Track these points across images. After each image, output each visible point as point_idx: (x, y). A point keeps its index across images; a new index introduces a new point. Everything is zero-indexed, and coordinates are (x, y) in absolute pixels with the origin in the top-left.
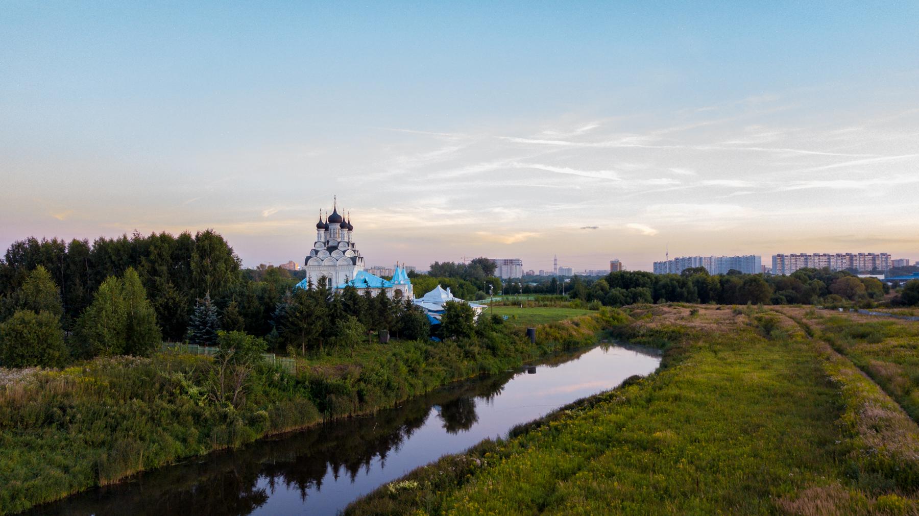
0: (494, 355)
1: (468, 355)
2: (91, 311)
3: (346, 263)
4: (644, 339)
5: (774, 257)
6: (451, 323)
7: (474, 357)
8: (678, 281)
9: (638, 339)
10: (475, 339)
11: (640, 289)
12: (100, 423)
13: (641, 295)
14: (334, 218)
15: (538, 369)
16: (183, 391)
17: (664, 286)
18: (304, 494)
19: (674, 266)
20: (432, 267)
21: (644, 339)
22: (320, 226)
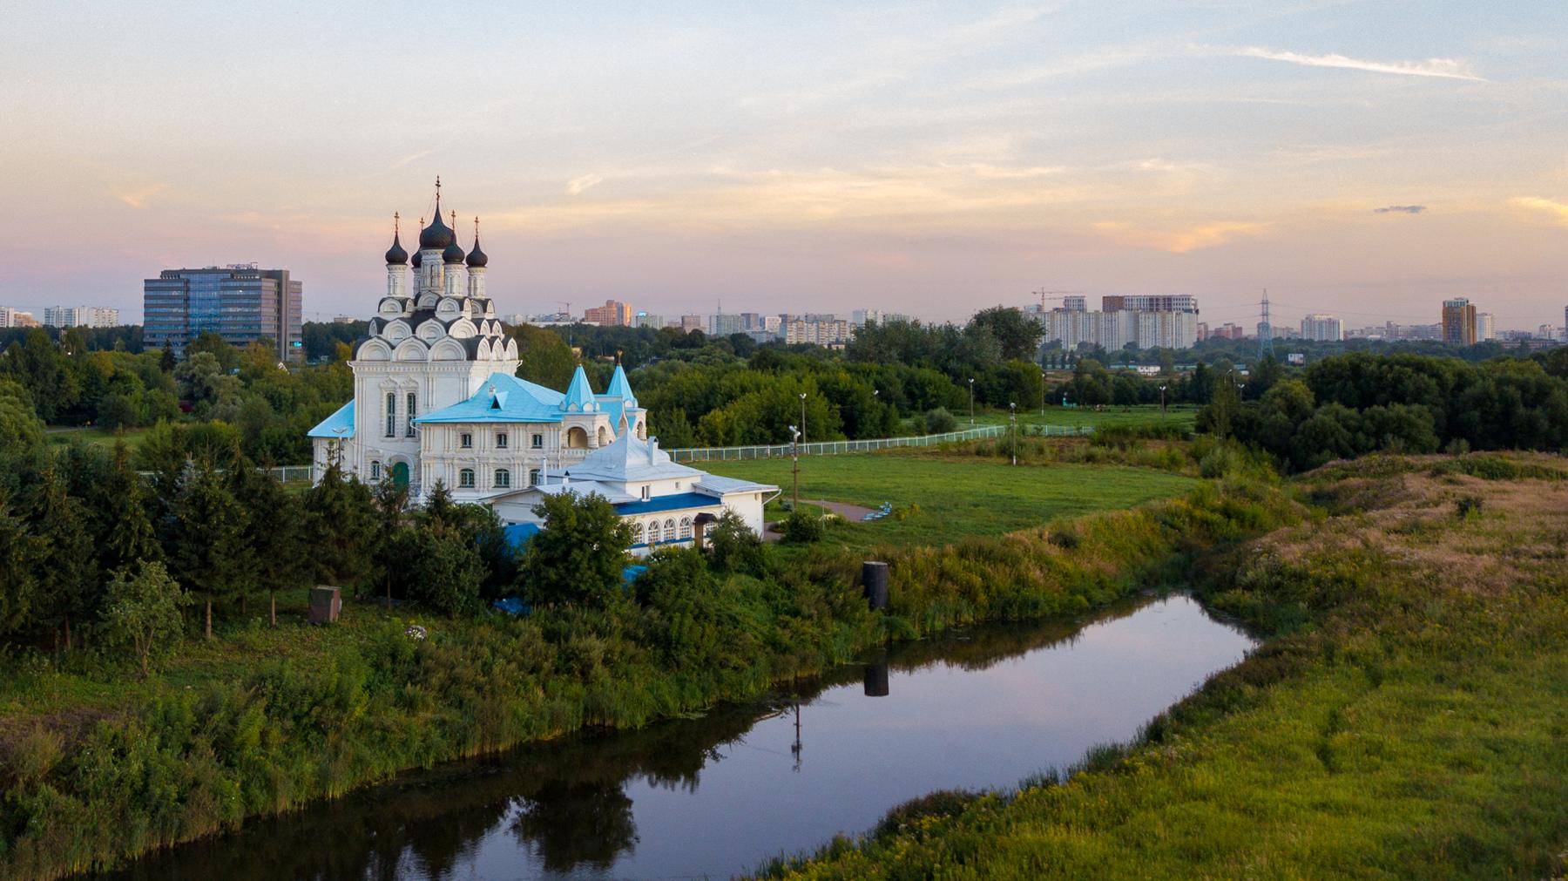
0: (667, 661)
3: (449, 355)
4: (1248, 598)
6: (550, 562)
8: (1523, 387)
9: (1233, 595)
10: (621, 609)
11: (1400, 409)
14: (437, 237)
15: (897, 679)
17: (1481, 401)
20: (858, 332)
21: (1248, 598)
22: (395, 257)
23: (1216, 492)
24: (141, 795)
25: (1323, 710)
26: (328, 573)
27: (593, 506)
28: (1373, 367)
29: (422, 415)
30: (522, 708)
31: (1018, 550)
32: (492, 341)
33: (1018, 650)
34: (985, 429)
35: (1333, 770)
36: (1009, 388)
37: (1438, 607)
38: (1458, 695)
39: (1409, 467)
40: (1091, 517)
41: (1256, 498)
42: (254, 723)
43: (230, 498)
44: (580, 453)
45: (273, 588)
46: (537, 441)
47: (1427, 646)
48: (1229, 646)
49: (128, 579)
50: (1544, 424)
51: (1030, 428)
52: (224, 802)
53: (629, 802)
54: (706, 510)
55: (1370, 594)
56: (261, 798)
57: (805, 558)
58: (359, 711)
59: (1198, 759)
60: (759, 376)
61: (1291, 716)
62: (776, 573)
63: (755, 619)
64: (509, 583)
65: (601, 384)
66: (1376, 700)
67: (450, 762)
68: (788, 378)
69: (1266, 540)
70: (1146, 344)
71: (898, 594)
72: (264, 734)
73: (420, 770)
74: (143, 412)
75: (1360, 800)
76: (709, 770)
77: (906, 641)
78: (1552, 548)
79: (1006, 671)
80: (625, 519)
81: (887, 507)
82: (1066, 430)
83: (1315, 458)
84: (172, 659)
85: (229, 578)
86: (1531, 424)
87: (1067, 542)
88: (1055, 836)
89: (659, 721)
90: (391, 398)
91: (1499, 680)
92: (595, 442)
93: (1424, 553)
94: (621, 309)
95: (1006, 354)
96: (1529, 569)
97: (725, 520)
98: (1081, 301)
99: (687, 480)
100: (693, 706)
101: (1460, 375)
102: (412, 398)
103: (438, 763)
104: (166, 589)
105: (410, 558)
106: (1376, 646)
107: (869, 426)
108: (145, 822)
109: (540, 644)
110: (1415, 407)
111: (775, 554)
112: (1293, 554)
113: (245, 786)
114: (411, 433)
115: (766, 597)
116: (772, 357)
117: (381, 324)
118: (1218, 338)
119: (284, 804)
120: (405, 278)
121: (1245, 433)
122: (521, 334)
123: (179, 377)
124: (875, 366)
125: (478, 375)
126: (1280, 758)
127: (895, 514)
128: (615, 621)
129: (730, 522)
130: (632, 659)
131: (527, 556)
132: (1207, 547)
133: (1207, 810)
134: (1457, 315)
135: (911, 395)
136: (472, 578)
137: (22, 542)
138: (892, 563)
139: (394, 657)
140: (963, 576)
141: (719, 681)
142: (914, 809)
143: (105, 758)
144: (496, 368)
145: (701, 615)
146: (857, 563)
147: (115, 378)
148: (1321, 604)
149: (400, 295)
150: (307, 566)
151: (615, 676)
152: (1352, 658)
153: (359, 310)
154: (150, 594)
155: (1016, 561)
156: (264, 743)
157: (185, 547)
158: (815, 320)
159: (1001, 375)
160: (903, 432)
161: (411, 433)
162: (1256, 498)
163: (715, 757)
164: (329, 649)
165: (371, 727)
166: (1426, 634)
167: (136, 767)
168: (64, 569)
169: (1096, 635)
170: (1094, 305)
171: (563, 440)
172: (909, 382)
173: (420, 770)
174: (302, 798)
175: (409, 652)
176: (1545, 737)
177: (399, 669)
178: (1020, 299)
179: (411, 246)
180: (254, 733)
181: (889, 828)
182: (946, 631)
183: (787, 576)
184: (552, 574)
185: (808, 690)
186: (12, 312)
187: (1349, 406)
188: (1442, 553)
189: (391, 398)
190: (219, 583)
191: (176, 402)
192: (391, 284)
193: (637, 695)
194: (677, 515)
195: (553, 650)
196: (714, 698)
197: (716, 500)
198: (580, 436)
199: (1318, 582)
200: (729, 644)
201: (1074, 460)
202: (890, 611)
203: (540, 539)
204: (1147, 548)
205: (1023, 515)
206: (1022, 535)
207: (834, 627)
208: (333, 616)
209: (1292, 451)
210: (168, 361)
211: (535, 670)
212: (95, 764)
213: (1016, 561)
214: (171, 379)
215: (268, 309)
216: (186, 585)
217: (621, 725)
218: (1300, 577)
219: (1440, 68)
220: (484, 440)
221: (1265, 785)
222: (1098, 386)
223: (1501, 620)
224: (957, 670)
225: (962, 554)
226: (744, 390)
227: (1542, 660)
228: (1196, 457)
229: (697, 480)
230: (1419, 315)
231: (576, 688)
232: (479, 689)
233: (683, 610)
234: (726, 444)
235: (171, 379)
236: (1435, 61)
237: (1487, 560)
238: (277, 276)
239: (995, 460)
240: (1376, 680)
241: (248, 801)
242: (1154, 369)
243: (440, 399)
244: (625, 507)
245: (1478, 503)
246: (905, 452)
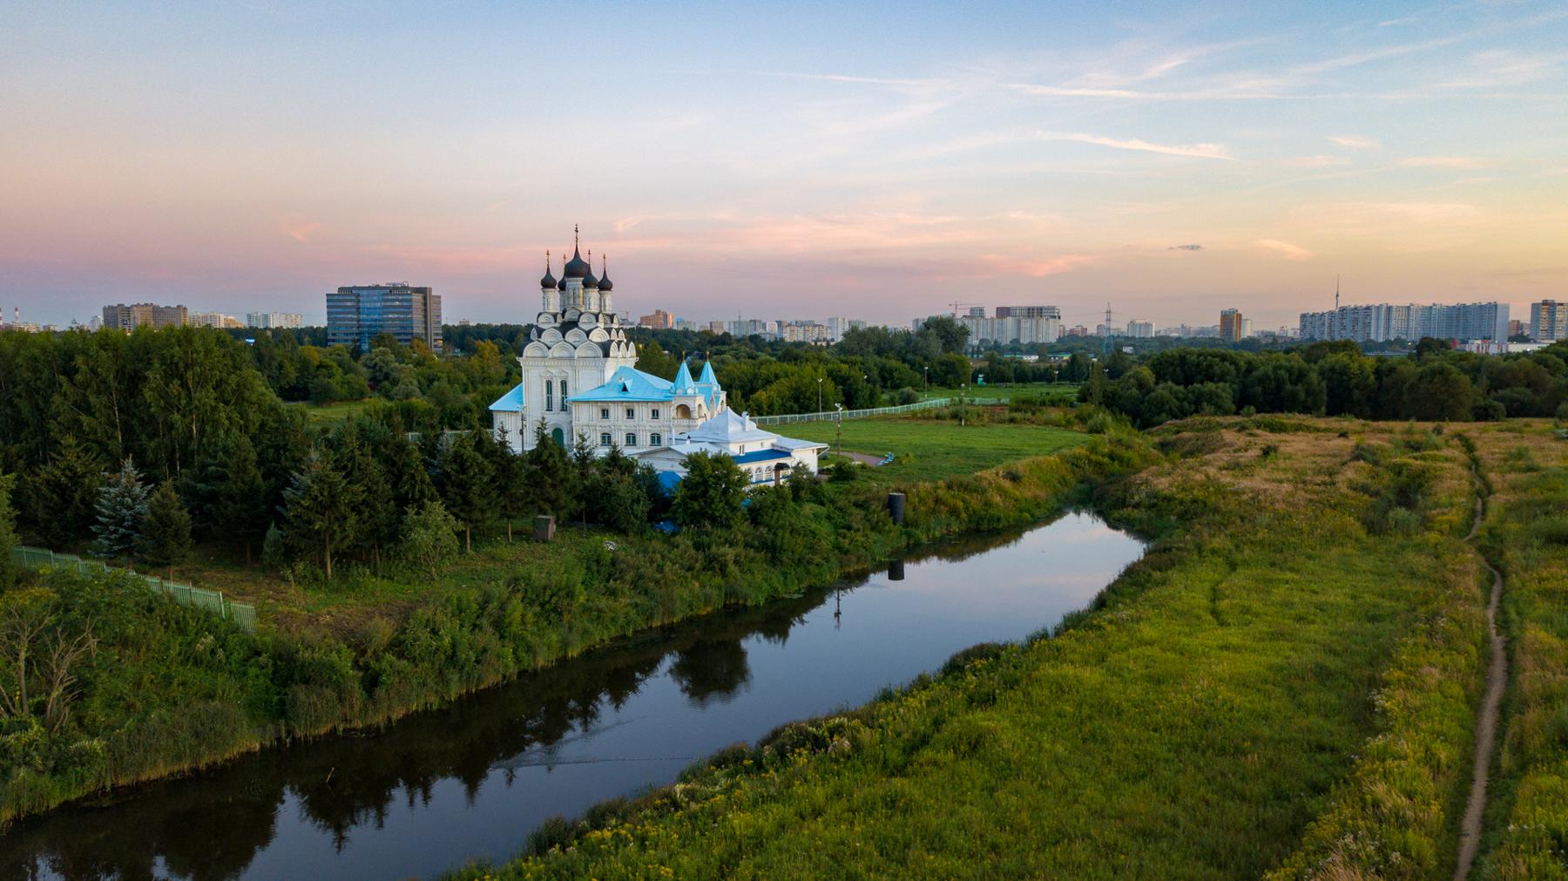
0: (774, 561)
1: (715, 565)
3: (590, 353)
4: (1135, 513)
5: (1535, 307)
6: (694, 498)
8: (1290, 371)
9: (1125, 512)
10: (741, 529)
11: (1210, 386)
13: (1211, 398)
14: (576, 268)
15: (909, 568)
17: (1261, 380)
18: (340, 839)
19: (1337, 323)
21: (1135, 513)
22: (547, 283)
23: (1104, 442)
24: (452, 658)
25: (1207, 585)
26: (547, 507)
27: (719, 460)
28: (1194, 358)
29: (571, 396)
30: (686, 594)
31: (985, 483)
32: (619, 343)
34: (937, 401)
35: (1222, 624)
36: (947, 373)
37: (1265, 518)
38: (1289, 575)
39: (1220, 425)
40: (1027, 460)
41: (1128, 447)
42: (516, 608)
43: (480, 458)
44: (685, 422)
45: (509, 517)
46: (655, 414)
47: (1261, 543)
49: (418, 513)
50: (1302, 395)
51: (966, 400)
52: (503, 664)
54: (782, 461)
55: (1216, 510)
56: (526, 659)
57: (849, 492)
58: (582, 599)
59: (1139, 620)
60: (786, 366)
61: (1189, 588)
62: (832, 502)
64: (666, 511)
65: (696, 373)
66: (1240, 578)
67: (643, 631)
68: (808, 368)
69: (1144, 475)
70: (1025, 340)
71: (911, 514)
72: (523, 616)
73: (624, 637)
74: (343, 391)
75: (1249, 643)
76: (796, 630)
77: (918, 544)
78: (1327, 479)
79: (975, 562)
80: (743, 467)
81: (890, 456)
82: (992, 400)
83: (1156, 419)
84: (447, 566)
85: (483, 511)
86: (1294, 395)
87: (1014, 478)
88: (1068, 670)
89: (773, 600)
90: (549, 384)
91: (1310, 564)
92: (695, 415)
93: (1245, 483)
94: (666, 316)
95: (946, 351)
96: (1314, 492)
97: (796, 468)
98: (981, 310)
99: (768, 440)
100: (792, 591)
101: (1249, 363)
102: (564, 384)
103: (636, 632)
104: (446, 520)
105: (587, 493)
106: (1229, 544)
107: (861, 400)
108: (456, 677)
109: (693, 552)
110: (1221, 384)
111: (828, 489)
112: (1163, 484)
113: (515, 652)
114: (564, 408)
115: (828, 517)
116: (791, 353)
117: (540, 332)
118: (1072, 336)
119: (541, 662)
120: (554, 296)
121: (1111, 402)
122: (634, 335)
123: (365, 365)
124: (859, 358)
125: (611, 368)
126: (1188, 616)
127: (898, 461)
128: (739, 536)
129: (800, 469)
130: (752, 560)
131: (679, 494)
132: (1100, 480)
133: (1155, 651)
134: (1230, 320)
135: (884, 379)
136: (642, 508)
137: (345, 490)
139: (598, 562)
140: (951, 501)
141: (808, 573)
143: (424, 635)
144: (622, 363)
146: (883, 494)
147: (320, 366)
148: (1185, 517)
149: (552, 310)
150: (532, 502)
151: (742, 571)
152: (1214, 552)
153: (519, 318)
154: (434, 524)
155: (984, 491)
156: (523, 623)
157: (451, 491)
158: (803, 325)
159: (942, 364)
160: (885, 404)
161: (564, 408)
162: (1128, 447)
163: (802, 622)
164: (556, 557)
165: (590, 609)
166: (1260, 536)
167: (447, 640)
168: (373, 507)
170: (990, 313)
171: (673, 413)
172: (882, 369)
173: (624, 637)
174: (553, 658)
175: (609, 557)
176: (1349, 601)
177: (605, 571)
178: (943, 312)
179: (558, 275)
180: (517, 615)
181: (954, 668)
182: (941, 539)
183: (840, 504)
184: (696, 505)
185: (860, 577)
186: (222, 317)
187: (1178, 383)
188: (1257, 482)
189: (549, 384)
190: (476, 515)
191: (366, 383)
192: (546, 303)
194: (764, 465)
195: (701, 556)
196: (805, 584)
197: (788, 454)
198: (685, 411)
199: (1181, 502)
200: (812, 548)
201: (1002, 422)
202: (906, 525)
203: (686, 483)
204: (1063, 481)
205: (983, 461)
206: (988, 474)
207: (874, 536)
208: (550, 535)
209: (1142, 415)
210: (356, 353)
211: (690, 569)
212: (419, 639)
213: (984, 491)
214: (359, 366)
215: (417, 316)
216: (457, 517)
217: (749, 603)
218: (1169, 499)
219: (1207, 150)
220: (617, 413)
221: (1186, 634)
222: (1001, 370)
223: (1304, 526)
224: (945, 562)
225: (949, 487)
226: (777, 377)
227: (1335, 552)
228: (1082, 419)
229: (775, 441)
230: (1206, 321)
231: (718, 580)
232: (657, 582)
233: (782, 527)
234: (769, 414)
235: (359, 366)
236: (1203, 145)
237: (1287, 487)
238: (423, 291)
239: (948, 422)
240: (1233, 566)
241: (518, 660)
242: (1035, 358)
243: (584, 384)
245: (1275, 449)
246: (887, 418)
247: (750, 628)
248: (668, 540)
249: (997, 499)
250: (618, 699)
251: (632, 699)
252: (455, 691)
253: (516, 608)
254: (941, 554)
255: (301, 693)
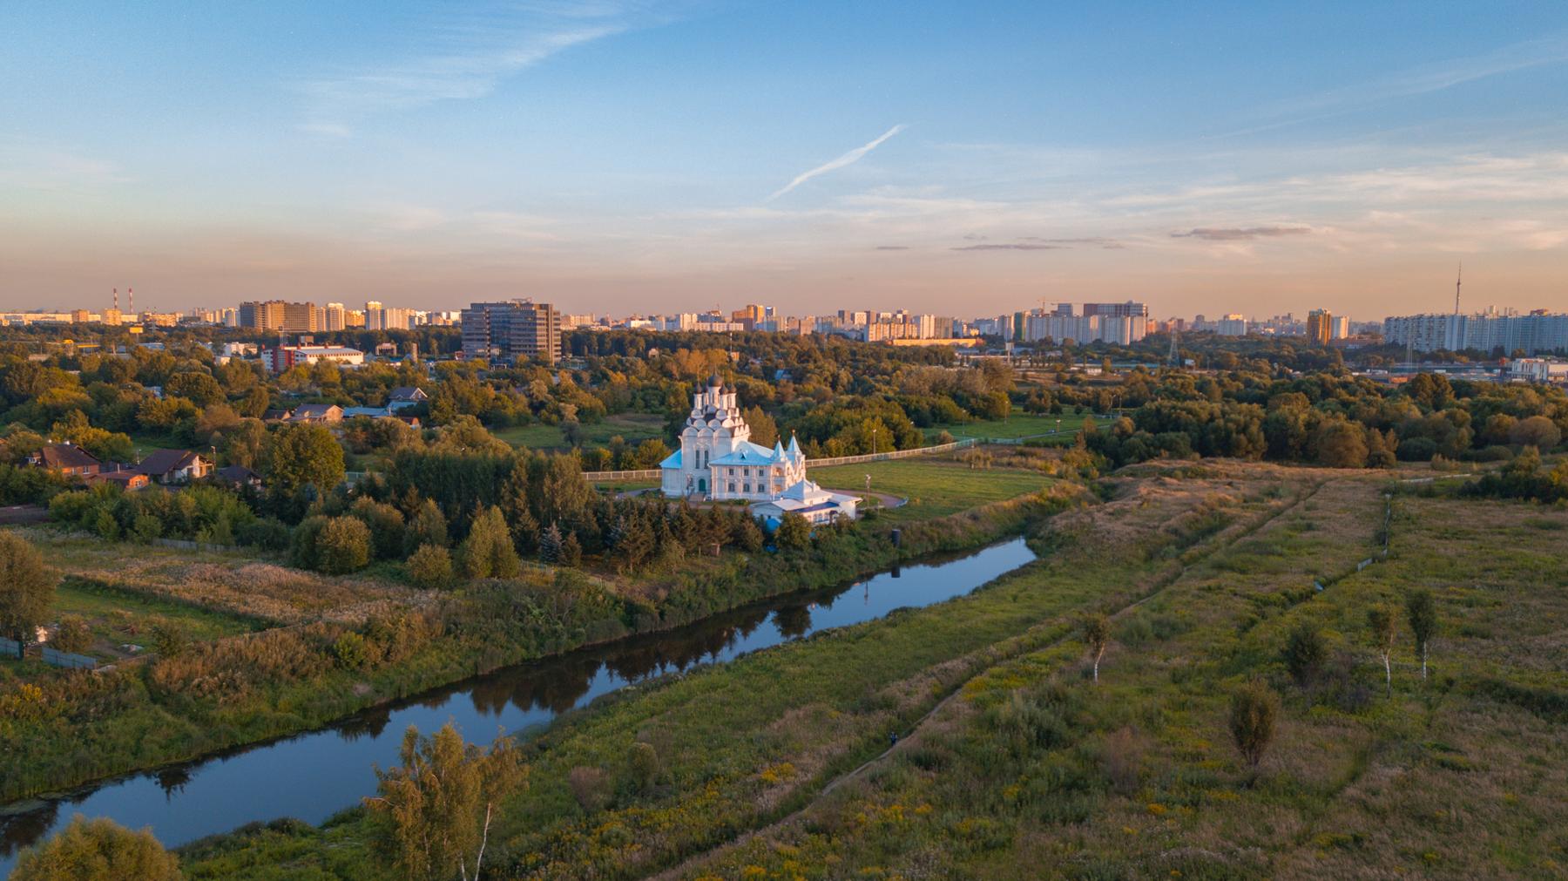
0: (824, 567)
2: (468, 543)
7: (798, 572)
10: (808, 550)
11: (1172, 435)
12: (477, 636)
15: (903, 571)
16: (529, 612)
33: (951, 560)
42: (710, 587)
48: (1029, 557)
52: (708, 610)
53: (498, 711)
63: (852, 552)
71: (905, 540)
87: (975, 518)
89: (822, 587)
98: (1069, 307)
100: (832, 582)
111: (858, 528)
129: (843, 515)
136: (760, 541)
138: (903, 529)
142: (895, 611)
145: (835, 552)
169: (986, 553)
170: (1078, 311)
185: (870, 576)
193: (815, 578)
200: (844, 561)
224: (928, 568)
238: (544, 307)
244: (803, 510)
247: (810, 601)
248: (772, 556)
249: (959, 532)
250: (745, 634)
251: (752, 634)
252: (691, 619)
253: (710, 587)
254: (925, 563)
255: (639, 617)
